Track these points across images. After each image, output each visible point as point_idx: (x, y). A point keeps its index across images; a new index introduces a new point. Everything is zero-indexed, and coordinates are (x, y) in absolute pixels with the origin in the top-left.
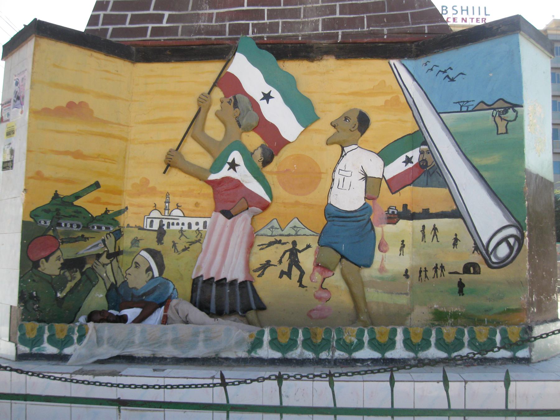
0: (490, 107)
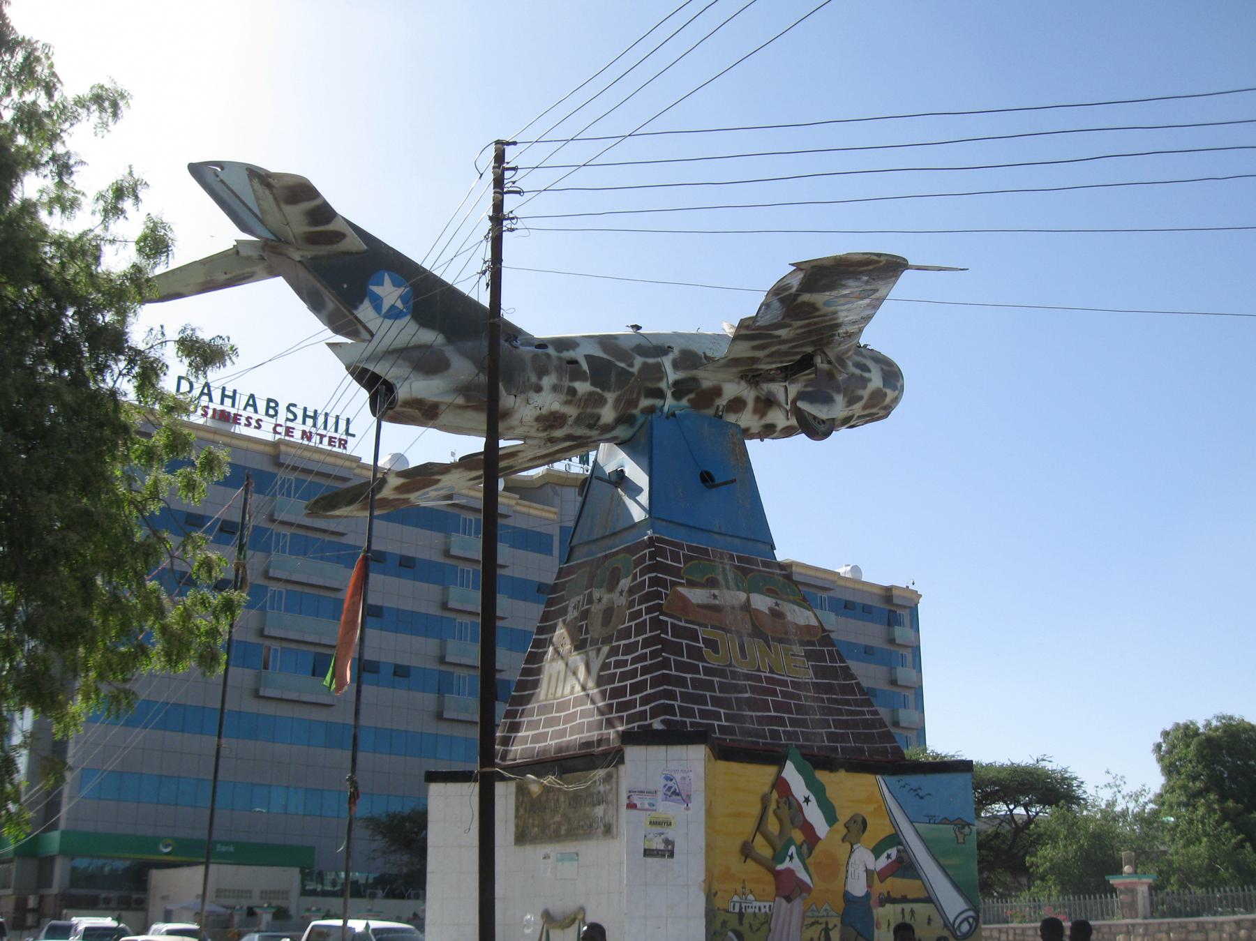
0: (951, 823)
